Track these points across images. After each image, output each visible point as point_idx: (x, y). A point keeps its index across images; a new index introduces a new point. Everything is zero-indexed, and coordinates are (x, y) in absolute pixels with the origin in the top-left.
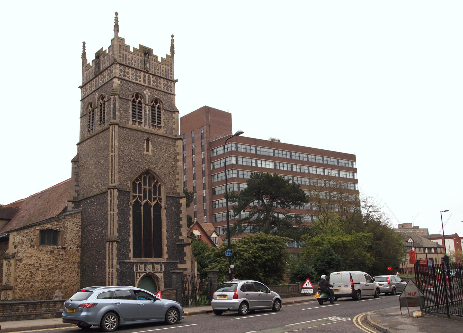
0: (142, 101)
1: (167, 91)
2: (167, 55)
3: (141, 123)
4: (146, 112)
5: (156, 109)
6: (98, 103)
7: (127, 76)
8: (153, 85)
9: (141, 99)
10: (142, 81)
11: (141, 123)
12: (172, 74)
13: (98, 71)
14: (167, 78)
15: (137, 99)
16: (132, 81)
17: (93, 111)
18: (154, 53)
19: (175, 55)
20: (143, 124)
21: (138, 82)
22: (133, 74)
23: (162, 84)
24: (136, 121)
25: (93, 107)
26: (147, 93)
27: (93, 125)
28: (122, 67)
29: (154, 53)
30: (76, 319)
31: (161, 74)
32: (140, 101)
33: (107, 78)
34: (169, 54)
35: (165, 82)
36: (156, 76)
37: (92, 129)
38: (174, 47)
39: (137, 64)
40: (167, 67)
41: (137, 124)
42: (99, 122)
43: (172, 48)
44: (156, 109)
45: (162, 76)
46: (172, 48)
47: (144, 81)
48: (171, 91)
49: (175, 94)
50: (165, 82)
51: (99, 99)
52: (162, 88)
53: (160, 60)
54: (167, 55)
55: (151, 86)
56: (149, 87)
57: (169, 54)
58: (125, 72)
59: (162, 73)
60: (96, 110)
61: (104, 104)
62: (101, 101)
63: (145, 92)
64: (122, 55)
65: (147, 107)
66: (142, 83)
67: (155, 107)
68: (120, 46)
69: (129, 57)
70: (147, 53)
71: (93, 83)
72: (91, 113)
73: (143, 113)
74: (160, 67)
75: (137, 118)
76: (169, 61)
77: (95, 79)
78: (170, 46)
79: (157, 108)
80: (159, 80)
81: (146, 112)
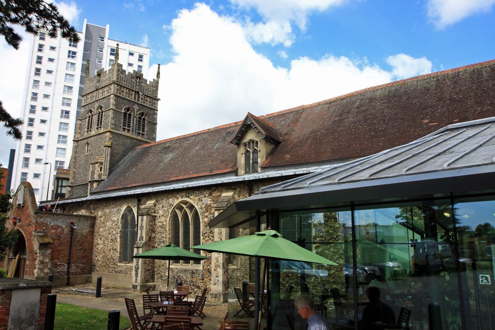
0: (132, 114)
1: (120, 95)
2: (154, 80)
3: (130, 130)
4: (134, 122)
5: (127, 116)
6: (97, 111)
7: (131, 97)
8: (141, 102)
9: (145, 116)
10: (133, 98)
11: (130, 130)
12: (157, 94)
13: (98, 86)
14: (121, 84)
15: (128, 112)
16: (126, 98)
17: (92, 117)
18: (144, 77)
19: (160, 80)
20: (131, 132)
21: (129, 99)
22: (126, 93)
23: (125, 92)
24: (140, 133)
25: (92, 113)
26: (136, 107)
27: (91, 128)
28: (119, 86)
29: (143, 77)
30: (484, 126)
31: (148, 94)
32: (144, 118)
33: (106, 94)
34: (156, 78)
35: (127, 91)
36: (152, 98)
37: (90, 131)
38: (159, 74)
39: (151, 93)
40: (153, 88)
41: (126, 131)
42: (96, 126)
43: (158, 73)
44: (127, 116)
45: (149, 95)
46: (158, 73)
47: (135, 99)
48: (155, 107)
49: (158, 109)
50: (127, 91)
51: (98, 109)
52: (148, 104)
53: (148, 83)
54: (154, 80)
55: (139, 103)
56: (138, 104)
57: (156, 78)
58: (152, 103)
59: (149, 92)
60: (95, 116)
61: (102, 113)
62: (100, 110)
63: (134, 107)
64: (119, 78)
65: (135, 118)
66: (133, 100)
67: (127, 114)
68: (118, 70)
69: (125, 79)
70: (139, 77)
71: (94, 94)
72: (91, 118)
73: (132, 121)
74: (148, 88)
75: (127, 127)
76: (156, 84)
77: (95, 92)
78: (157, 72)
79: (129, 115)
80: (146, 98)
81: (134, 122)
